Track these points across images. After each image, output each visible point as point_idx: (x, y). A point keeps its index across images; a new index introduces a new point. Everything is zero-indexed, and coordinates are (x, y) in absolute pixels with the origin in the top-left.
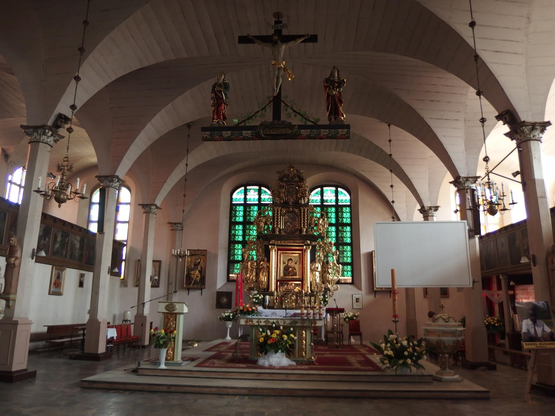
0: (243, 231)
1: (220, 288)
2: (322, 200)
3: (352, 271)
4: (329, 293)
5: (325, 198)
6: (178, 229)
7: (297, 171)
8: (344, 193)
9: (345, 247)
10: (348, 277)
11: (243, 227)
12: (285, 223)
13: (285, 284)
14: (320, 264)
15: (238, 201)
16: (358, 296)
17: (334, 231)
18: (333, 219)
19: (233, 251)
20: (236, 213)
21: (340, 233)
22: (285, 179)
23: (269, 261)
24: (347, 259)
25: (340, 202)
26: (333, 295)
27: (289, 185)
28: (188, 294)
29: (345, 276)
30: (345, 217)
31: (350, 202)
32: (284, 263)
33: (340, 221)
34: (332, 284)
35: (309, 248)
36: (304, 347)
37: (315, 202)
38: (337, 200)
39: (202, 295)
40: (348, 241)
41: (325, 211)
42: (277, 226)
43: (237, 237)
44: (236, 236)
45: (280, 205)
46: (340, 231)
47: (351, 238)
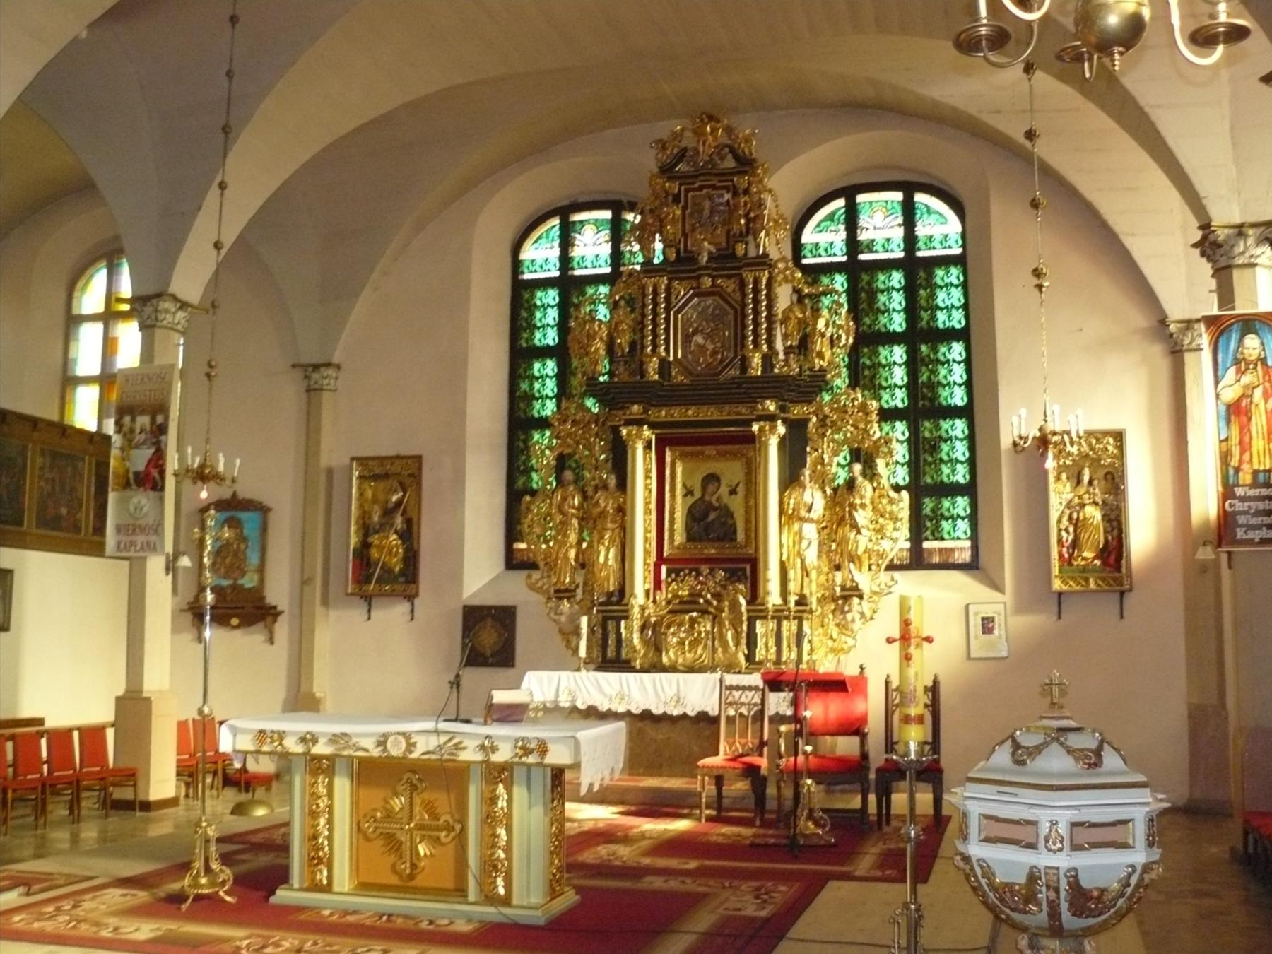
0: (557, 379)
1: (474, 595)
2: (853, 245)
3: (973, 519)
4: (860, 604)
5: (863, 236)
6: (328, 384)
7: (729, 130)
8: (937, 212)
9: (945, 425)
10: (958, 542)
11: (558, 365)
12: (687, 338)
13: (687, 571)
14: (824, 492)
15: (538, 269)
16: (988, 611)
17: (899, 361)
18: (895, 315)
19: (524, 457)
20: (532, 315)
21: (924, 369)
22: (681, 167)
23: (623, 483)
24: (954, 471)
25: (923, 247)
26: (875, 612)
27: (701, 188)
28: (366, 617)
29: (946, 536)
30: (941, 305)
31: (960, 242)
32: (688, 492)
33: (924, 323)
34: (870, 569)
35: (773, 429)
36: (502, 855)
37: (823, 253)
38: (910, 240)
39: (412, 619)
40: (958, 397)
41: (866, 287)
42: (654, 350)
43: (537, 405)
44: (535, 403)
45: (664, 270)
46: (922, 360)
47: (969, 385)
